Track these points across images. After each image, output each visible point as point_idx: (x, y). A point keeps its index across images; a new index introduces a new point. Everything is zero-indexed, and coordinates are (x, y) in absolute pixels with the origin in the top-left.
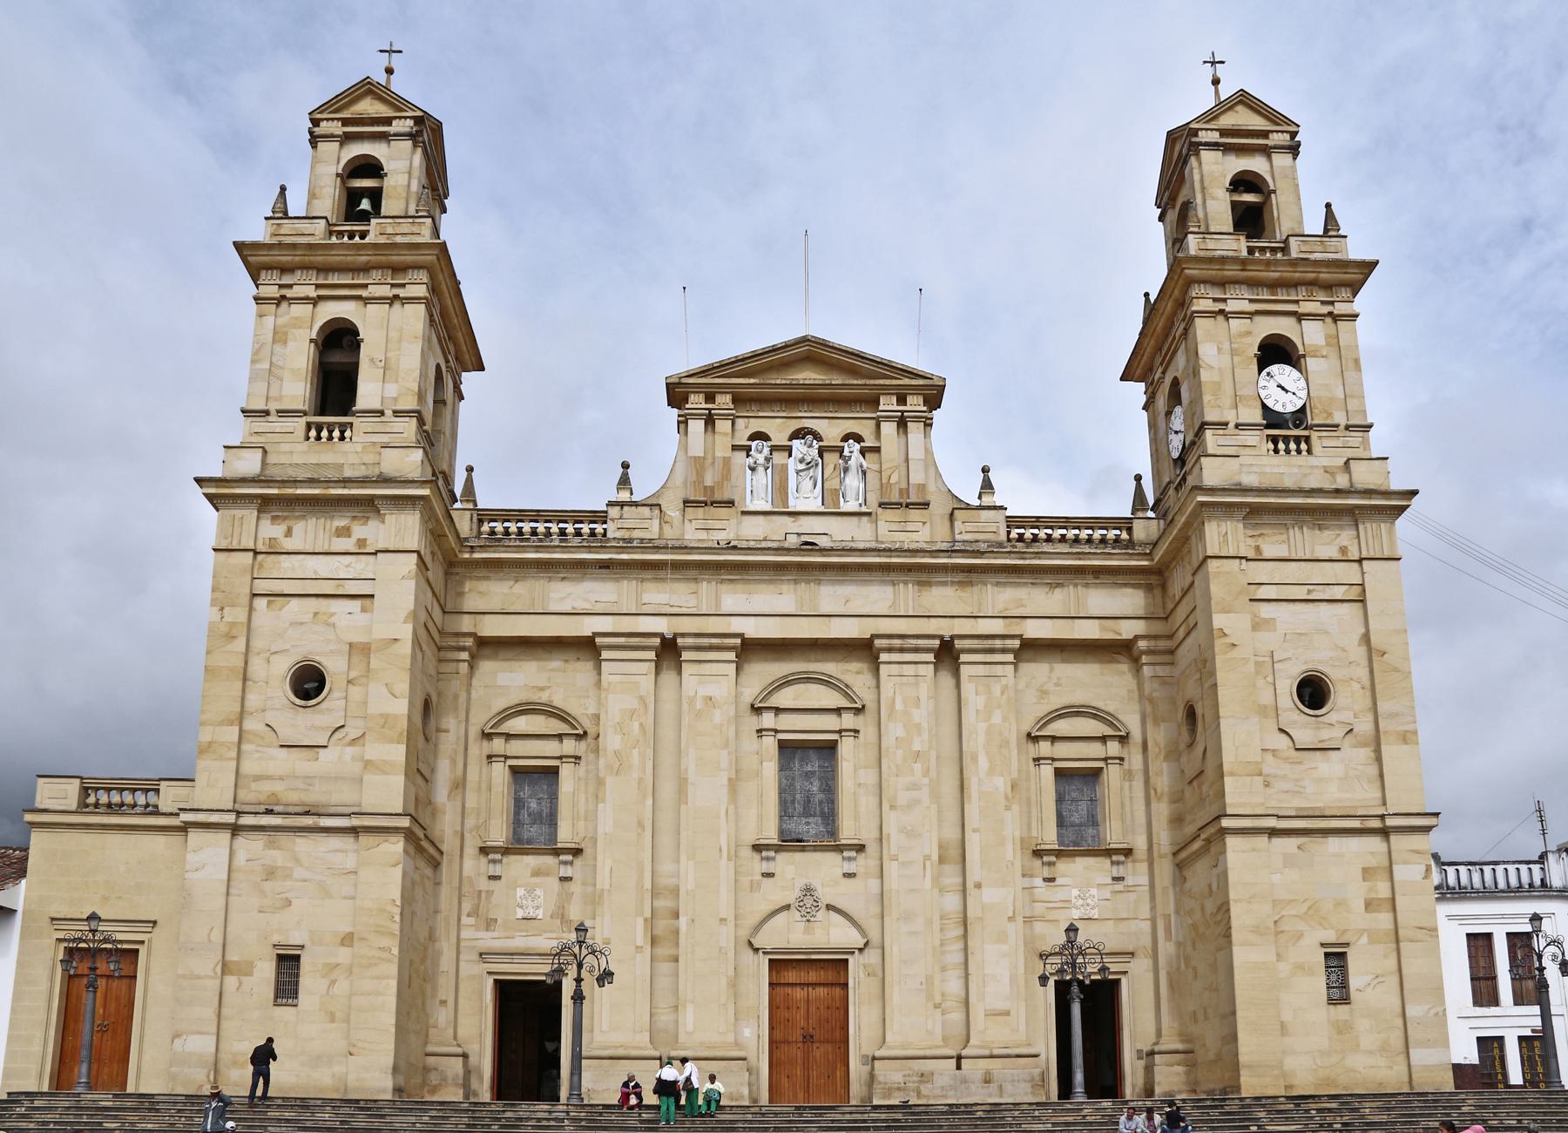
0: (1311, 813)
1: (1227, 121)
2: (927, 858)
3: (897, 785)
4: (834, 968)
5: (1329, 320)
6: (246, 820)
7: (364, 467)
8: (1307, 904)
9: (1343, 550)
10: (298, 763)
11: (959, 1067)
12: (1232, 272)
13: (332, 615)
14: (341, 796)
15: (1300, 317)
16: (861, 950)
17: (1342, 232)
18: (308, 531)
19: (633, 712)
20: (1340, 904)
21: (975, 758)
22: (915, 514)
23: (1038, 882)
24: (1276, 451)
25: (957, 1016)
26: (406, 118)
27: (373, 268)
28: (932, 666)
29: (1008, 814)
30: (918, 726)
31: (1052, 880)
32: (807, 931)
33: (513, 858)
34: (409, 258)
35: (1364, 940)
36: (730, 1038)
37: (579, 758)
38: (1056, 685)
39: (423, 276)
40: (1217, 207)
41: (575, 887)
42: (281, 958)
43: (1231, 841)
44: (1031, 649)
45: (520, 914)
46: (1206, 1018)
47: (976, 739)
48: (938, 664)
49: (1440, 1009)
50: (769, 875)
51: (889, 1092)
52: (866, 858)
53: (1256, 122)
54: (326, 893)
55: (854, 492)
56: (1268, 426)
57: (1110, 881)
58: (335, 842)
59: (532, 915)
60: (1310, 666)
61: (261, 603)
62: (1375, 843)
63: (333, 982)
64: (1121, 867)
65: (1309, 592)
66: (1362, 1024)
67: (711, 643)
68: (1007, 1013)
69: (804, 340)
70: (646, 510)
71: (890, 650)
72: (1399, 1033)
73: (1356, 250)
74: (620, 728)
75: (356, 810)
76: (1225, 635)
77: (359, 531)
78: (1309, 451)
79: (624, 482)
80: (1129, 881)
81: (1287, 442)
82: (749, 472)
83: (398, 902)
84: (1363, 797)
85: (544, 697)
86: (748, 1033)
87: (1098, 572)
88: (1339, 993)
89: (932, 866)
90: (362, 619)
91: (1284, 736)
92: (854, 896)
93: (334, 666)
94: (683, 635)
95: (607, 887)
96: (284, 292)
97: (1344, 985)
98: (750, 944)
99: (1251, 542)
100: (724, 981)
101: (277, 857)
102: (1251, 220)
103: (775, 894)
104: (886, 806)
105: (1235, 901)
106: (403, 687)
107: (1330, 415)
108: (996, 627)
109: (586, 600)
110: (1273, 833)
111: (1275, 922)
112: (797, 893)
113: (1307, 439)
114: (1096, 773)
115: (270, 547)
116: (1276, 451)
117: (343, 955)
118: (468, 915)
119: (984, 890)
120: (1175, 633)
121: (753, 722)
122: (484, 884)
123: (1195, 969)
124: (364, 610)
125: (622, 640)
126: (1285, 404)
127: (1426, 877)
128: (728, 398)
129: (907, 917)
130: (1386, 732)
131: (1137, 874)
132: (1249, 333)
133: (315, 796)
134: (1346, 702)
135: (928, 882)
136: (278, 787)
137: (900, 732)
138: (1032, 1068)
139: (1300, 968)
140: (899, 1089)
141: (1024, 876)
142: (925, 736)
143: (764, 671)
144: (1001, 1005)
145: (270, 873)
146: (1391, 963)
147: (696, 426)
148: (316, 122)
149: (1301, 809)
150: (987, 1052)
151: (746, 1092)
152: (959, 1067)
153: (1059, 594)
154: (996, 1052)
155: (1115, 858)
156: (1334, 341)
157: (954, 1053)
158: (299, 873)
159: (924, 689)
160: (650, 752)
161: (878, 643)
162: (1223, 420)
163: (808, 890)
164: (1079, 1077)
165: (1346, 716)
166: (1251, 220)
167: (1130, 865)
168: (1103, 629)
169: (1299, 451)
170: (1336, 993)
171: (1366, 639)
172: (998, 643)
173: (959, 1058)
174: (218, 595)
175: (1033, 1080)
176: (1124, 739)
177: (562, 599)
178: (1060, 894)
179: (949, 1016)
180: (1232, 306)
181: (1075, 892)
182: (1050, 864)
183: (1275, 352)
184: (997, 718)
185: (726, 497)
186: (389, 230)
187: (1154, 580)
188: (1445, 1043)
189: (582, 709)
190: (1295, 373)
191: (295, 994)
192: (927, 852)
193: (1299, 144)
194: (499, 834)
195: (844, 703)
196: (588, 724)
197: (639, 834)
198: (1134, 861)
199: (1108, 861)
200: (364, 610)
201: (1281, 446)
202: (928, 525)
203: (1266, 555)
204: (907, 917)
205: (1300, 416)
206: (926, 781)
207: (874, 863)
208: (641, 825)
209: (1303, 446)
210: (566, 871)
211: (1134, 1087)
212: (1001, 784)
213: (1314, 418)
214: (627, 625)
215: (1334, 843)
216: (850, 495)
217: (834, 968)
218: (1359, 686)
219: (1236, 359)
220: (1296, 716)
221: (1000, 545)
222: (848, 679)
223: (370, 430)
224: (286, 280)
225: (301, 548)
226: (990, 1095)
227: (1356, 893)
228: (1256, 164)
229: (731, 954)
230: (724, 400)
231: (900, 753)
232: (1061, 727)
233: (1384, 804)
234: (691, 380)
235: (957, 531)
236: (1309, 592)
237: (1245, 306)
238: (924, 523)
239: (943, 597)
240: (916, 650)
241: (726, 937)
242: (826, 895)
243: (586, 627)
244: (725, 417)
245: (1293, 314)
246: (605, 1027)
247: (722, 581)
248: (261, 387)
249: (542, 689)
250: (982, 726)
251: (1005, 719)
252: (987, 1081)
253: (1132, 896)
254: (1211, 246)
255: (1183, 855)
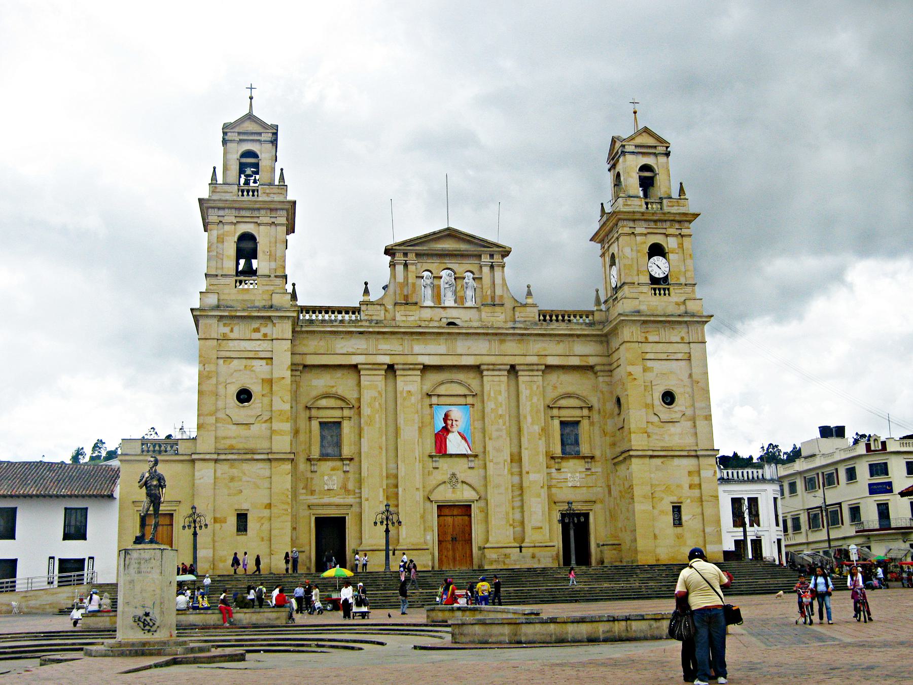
0: (667, 449)
1: (639, 140)
2: (505, 461)
3: (491, 429)
4: (466, 509)
5: (679, 236)
6: (222, 457)
7: (264, 301)
8: (665, 487)
9: (682, 338)
10: (242, 431)
11: (521, 551)
12: (638, 216)
13: (253, 366)
14: (264, 445)
15: (667, 236)
16: (477, 500)
17: (686, 197)
18: (240, 330)
19: (375, 398)
20: (679, 486)
21: (525, 417)
22: (497, 309)
23: (553, 470)
24: (655, 294)
25: (518, 529)
26: (268, 133)
27: (262, 209)
28: (506, 377)
29: (540, 441)
30: (501, 403)
31: (560, 469)
32: (453, 492)
33: (323, 463)
34: (279, 206)
35: (689, 500)
36: (422, 540)
37: (350, 418)
38: (561, 384)
39: (284, 213)
40: (632, 183)
41: (351, 475)
42: (238, 515)
43: (633, 460)
44: (549, 368)
45: (326, 487)
46: (626, 531)
47: (526, 408)
48: (509, 372)
49: (719, 529)
50: (437, 468)
51: (491, 563)
52: (478, 460)
53: (651, 141)
54: (257, 486)
55: (471, 297)
56: (651, 284)
57: (584, 470)
58: (260, 465)
59: (331, 488)
60: (668, 388)
61: (221, 361)
62: (693, 461)
63: (263, 524)
64: (590, 464)
65: (668, 356)
66: (687, 535)
67: (410, 367)
68: (541, 528)
69: (448, 229)
70: (379, 307)
71: (488, 370)
72: (702, 539)
73: (691, 207)
74: (370, 405)
75: (269, 451)
76: (632, 374)
77: (264, 330)
78: (669, 294)
79: (366, 292)
80: (593, 470)
81: (659, 289)
82: (423, 287)
83: (290, 490)
84: (688, 442)
85: (334, 390)
86: (429, 537)
87: (578, 336)
88: (678, 522)
89: (508, 464)
90: (268, 368)
91: (656, 416)
92: (474, 477)
93: (256, 389)
94: (397, 364)
95: (366, 475)
96: (221, 219)
97: (680, 519)
98: (429, 499)
99: (643, 335)
100: (419, 516)
101: (235, 472)
102: (647, 183)
103: (439, 476)
104: (487, 439)
105: (636, 485)
106: (288, 397)
107: (678, 279)
108: (534, 360)
109: (353, 348)
110: (651, 457)
111: (652, 494)
112: (449, 476)
113: (669, 289)
114: (578, 423)
115: (224, 337)
116: (655, 294)
117: (266, 513)
118: (303, 489)
119: (530, 474)
120: (615, 369)
121: (427, 401)
122: (309, 475)
123: (621, 510)
124: (267, 364)
125: (370, 366)
126: (658, 274)
127: (714, 475)
128: (414, 254)
129: (498, 486)
130: (698, 415)
131: (597, 468)
132: (645, 243)
133: (251, 445)
134: (681, 402)
135: (506, 470)
136: (233, 442)
137: (493, 406)
138: (553, 552)
139: (662, 512)
140: (496, 561)
141: (547, 468)
142: (504, 407)
143: (433, 378)
144: (539, 525)
145: (232, 479)
146: (699, 510)
147: (400, 268)
148: (225, 133)
149: (663, 447)
150: (533, 545)
151: (430, 564)
152: (521, 551)
153: (561, 345)
154: (537, 545)
155: (586, 460)
156: (681, 246)
157: (518, 545)
158: (245, 478)
159: (503, 387)
160: (384, 416)
161: (483, 367)
162: (632, 281)
163: (454, 475)
164: (573, 558)
165: (683, 408)
166: (647, 183)
167: (593, 463)
168: (581, 360)
169: (665, 294)
170: (677, 522)
171: (690, 376)
172: (535, 367)
173: (521, 547)
174: (202, 359)
175: (553, 556)
176: (590, 408)
177: (342, 347)
178: (563, 476)
179: (516, 529)
180: (637, 231)
181: (569, 475)
182: (558, 463)
183: (656, 250)
184: (535, 399)
185: (414, 301)
186: (268, 191)
187: (603, 339)
188: (720, 541)
189: (351, 395)
190: (664, 260)
191: (246, 530)
192: (506, 458)
193: (670, 152)
194: (316, 453)
195: (467, 392)
196: (354, 402)
197: (380, 452)
198: (595, 462)
199: (583, 461)
200: (267, 364)
201: (657, 292)
202: (504, 314)
203: (650, 340)
204: (498, 486)
205: (665, 279)
206: (504, 427)
207: (481, 462)
208: (381, 448)
209: (667, 292)
210: (346, 468)
211: (596, 559)
212: (537, 428)
213: (671, 281)
214: (372, 359)
215: (676, 461)
216: (469, 298)
217: (466, 509)
218: (688, 395)
219: (639, 254)
220: (661, 408)
221: (536, 324)
222: (470, 381)
223: (265, 284)
224: (221, 213)
225: (238, 337)
226: (535, 563)
227: (685, 481)
228: (650, 161)
229: (422, 503)
230: (412, 256)
231: (493, 415)
232: (563, 403)
233: (697, 445)
234: (397, 248)
235: (516, 317)
236: (668, 356)
237: (644, 231)
238: (502, 313)
239: (511, 347)
240: (500, 370)
241: (419, 496)
242: (461, 476)
243: (354, 360)
244: (413, 264)
245: (665, 234)
246: (367, 537)
247: (413, 340)
248: (213, 263)
249: (333, 387)
250: (528, 404)
251: (538, 400)
252: (533, 557)
253: (594, 477)
254: (629, 203)
255: (616, 460)
